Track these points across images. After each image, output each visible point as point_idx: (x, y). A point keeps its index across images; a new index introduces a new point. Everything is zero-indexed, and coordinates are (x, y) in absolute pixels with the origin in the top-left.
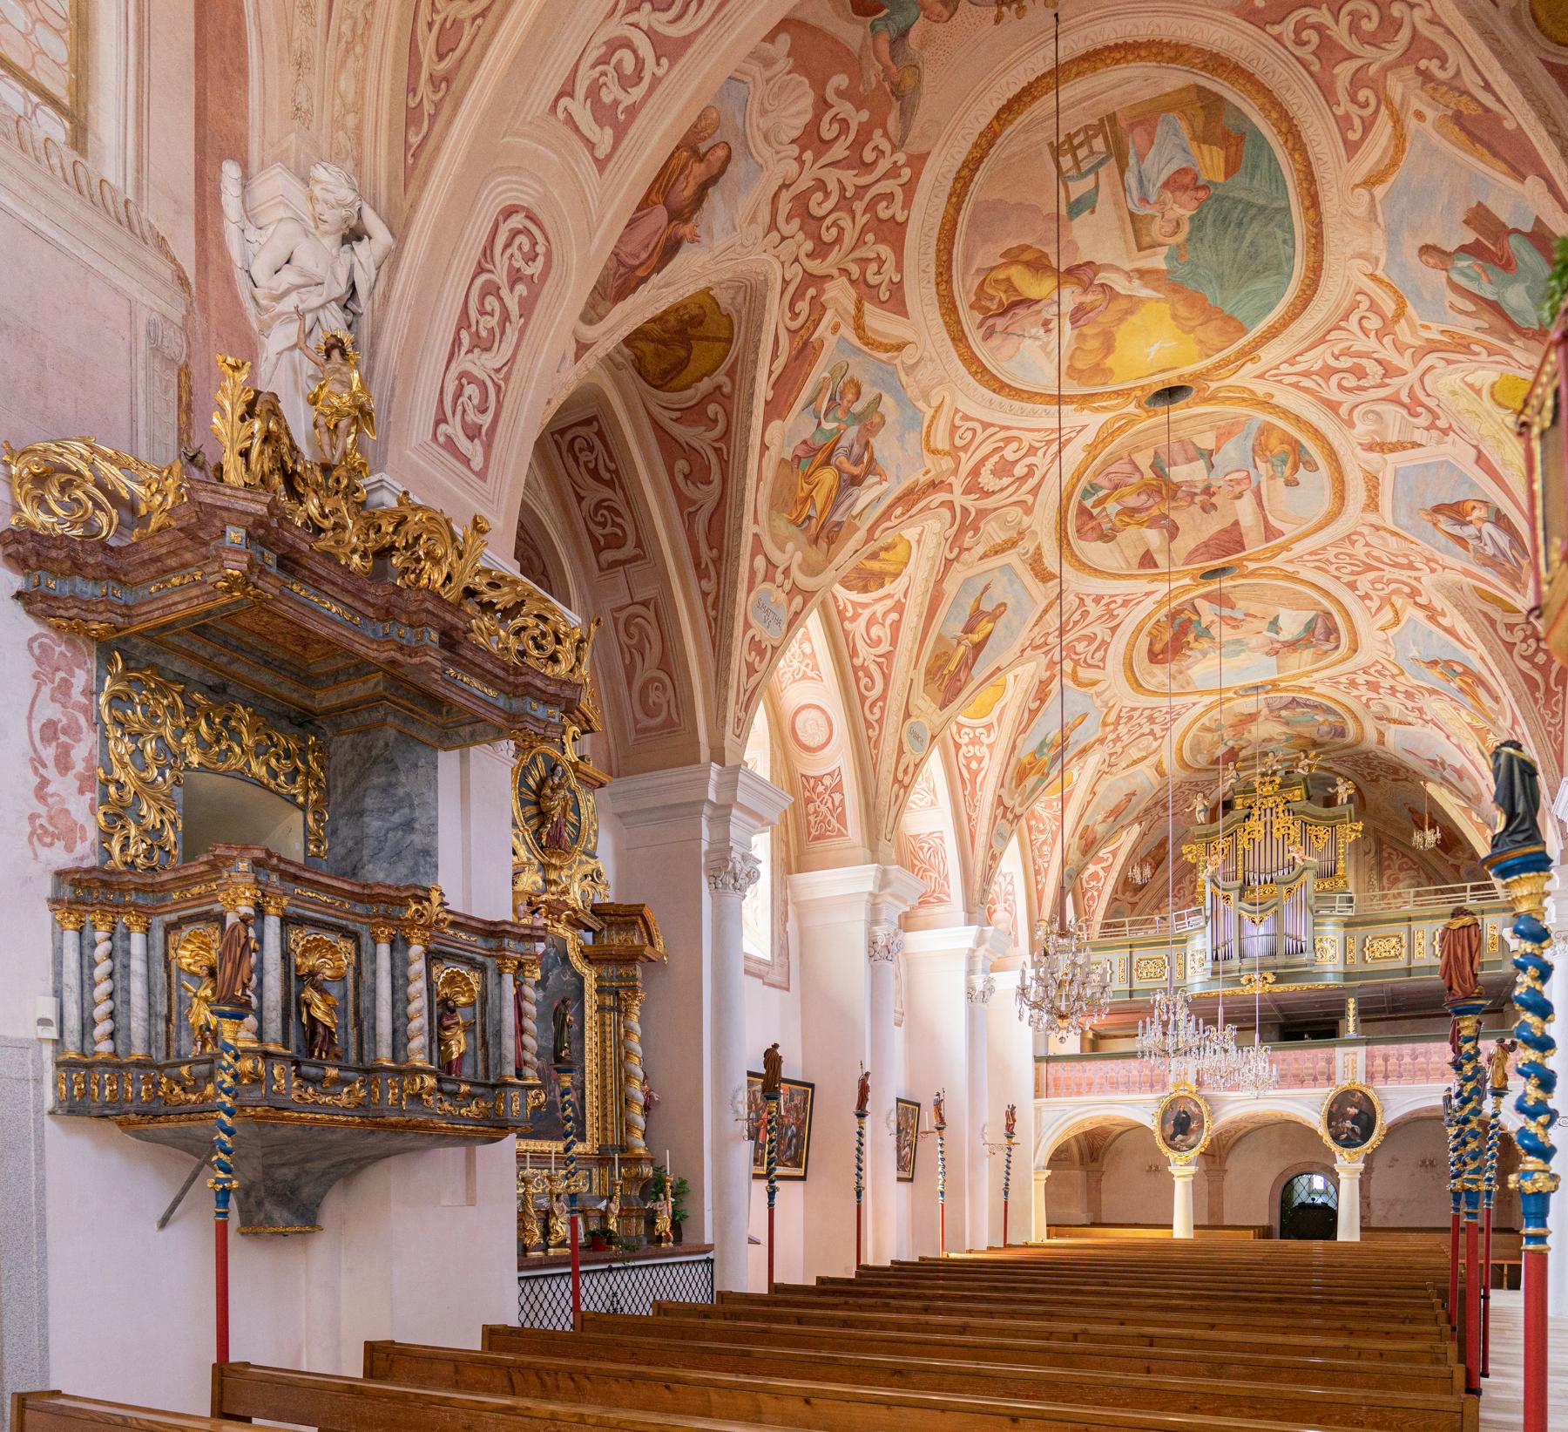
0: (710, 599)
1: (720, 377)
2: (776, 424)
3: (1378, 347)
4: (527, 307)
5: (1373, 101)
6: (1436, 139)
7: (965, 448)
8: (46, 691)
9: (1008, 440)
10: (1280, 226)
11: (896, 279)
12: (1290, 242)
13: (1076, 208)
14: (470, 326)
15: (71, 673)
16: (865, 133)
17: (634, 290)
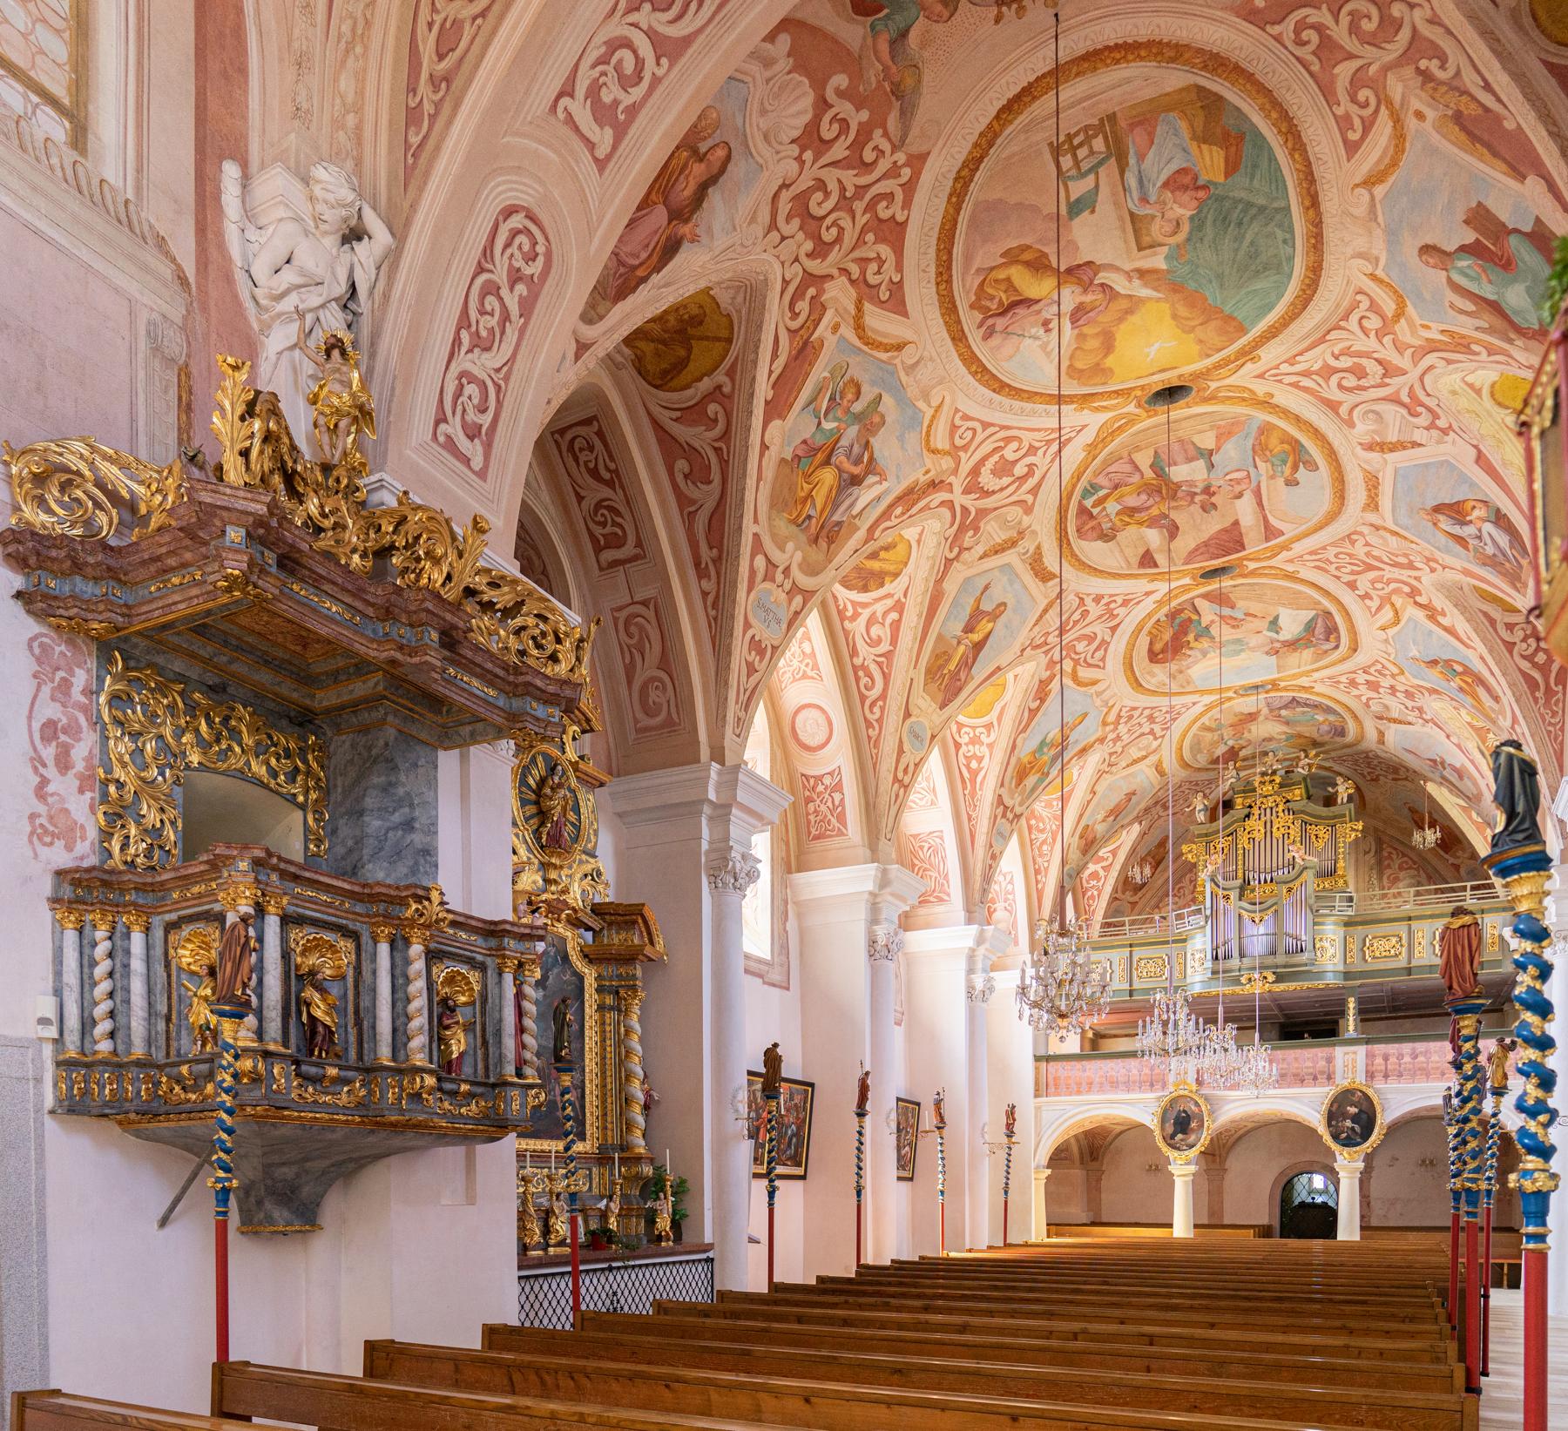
0: (710, 599)
1: (720, 377)
2: (776, 424)
3: (1378, 347)
4: (527, 307)
5: (1373, 101)
6: (1436, 138)
7: (965, 448)
8: (46, 690)
9: (1008, 440)
10: (1280, 226)
11: (896, 279)
12: (1290, 242)
13: (1076, 208)
14: (470, 326)
15: (71, 672)
16: (865, 133)
17: (634, 290)
